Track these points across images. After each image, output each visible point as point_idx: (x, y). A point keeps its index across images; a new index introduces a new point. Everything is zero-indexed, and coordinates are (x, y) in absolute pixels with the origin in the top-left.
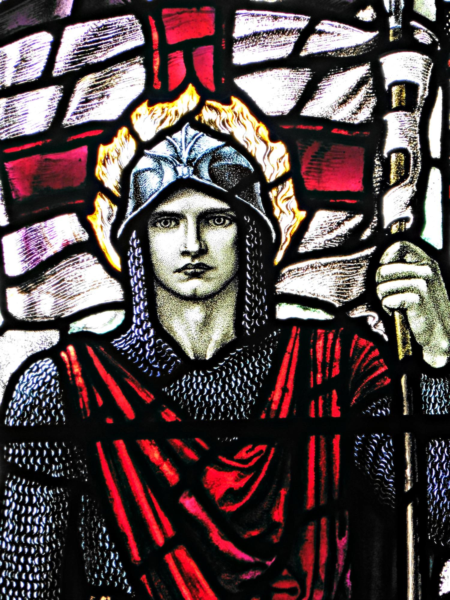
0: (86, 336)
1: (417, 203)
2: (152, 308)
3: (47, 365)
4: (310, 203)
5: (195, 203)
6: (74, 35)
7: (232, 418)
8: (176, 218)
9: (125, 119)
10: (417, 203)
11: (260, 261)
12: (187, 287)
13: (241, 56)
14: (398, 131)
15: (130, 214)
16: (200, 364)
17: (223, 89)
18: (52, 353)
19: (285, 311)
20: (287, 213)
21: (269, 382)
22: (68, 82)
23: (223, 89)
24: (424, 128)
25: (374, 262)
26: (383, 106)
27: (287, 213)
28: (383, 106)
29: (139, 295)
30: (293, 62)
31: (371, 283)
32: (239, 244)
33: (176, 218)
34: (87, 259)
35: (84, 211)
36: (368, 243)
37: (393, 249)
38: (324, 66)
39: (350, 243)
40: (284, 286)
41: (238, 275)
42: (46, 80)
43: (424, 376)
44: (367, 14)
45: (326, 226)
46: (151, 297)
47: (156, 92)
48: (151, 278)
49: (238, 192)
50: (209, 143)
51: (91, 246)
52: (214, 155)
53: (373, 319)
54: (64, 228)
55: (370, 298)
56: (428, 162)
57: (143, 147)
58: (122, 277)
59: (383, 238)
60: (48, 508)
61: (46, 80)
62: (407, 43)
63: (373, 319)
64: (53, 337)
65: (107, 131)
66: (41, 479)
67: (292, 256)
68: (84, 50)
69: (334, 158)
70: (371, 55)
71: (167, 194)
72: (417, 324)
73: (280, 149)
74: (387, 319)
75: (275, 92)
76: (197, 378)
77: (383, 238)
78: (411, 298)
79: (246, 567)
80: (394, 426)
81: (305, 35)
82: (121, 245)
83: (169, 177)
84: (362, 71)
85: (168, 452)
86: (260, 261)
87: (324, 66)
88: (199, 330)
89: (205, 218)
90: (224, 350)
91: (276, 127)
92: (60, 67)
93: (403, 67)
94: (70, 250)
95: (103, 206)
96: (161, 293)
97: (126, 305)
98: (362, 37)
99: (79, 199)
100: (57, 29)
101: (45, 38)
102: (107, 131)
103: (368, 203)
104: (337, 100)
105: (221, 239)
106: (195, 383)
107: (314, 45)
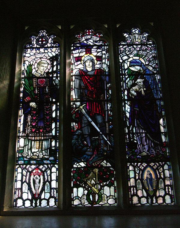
0: (81, 70)
1: (105, 61)
2: (86, 68)
3: (78, 71)
4: (97, 61)
5: (89, 61)
6: (80, 50)
7: (132, 140)
8: (87, 62)
9: (84, 56)
10: (105, 61)
11: (94, 65)
12: (88, 66)
13: (92, 52)
14: (104, 56)
15: (84, 61)
16: (89, 72)
17: (91, 53)
18: (79, 71)
19: (96, 68)
20: (96, 61)
21: (95, 73)
22: (80, 53)
23: (91, 53)
24: (106, 56)
25: (102, 65)
26: (103, 54)
27: (96, 61)
28: (103, 54)
29: (85, 67)
30: (96, 52)
31: (102, 66)
32: (92, 64)
33: (87, 62)
34: (81, 64)
35: (81, 61)
36: (101, 64)
37: (104, 64)
38: (98, 52)
39: (100, 63)
40: (95, 66)
41: (92, 66)
42: (78, 53)
43: (163, 188)
44: (101, 49)
45: (99, 62)
46: (86, 67)
47: (86, 54)
48: (86, 66)
49: (92, 60)
50: (90, 57)
51: (81, 64)
52: (90, 58)
53: (102, 68)
54: (79, 62)
55: (102, 67)
56: (106, 58)
57: (85, 57)
58: (84, 66)
59: (103, 63)
60: (97, 103)
61: (78, 53)
62: (104, 51)
63: (102, 68)
64: (78, 70)
65: (82, 56)
66: (78, 79)
67: (96, 64)
68: (81, 51)
69: (99, 58)
70: (102, 51)
71: (87, 60)
72: (105, 69)
73: (95, 57)
74: (103, 68)
75: (95, 54)
76: (89, 72)
77: (103, 63)
78: (105, 67)
79: (93, 85)
80: (104, 75)
81: (97, 50)
82: (84, 64)
83: (87, 59)
84: (101, 52)
85: (87, 77)
86: (94, 65)
87: (98, 52)
88: (89, 69)
89: (90, 62)
90: (91, 71)
91: (95, 56)
92: (79, 52)
93: (104, 52)
94: (80, 64)
95: (82, 61)
96: (86, 67)
97: (84, 67)
98: (101, 50)
99: (81, 60)
100: (79, 50)
101: (78, 50)
102: (82, 56)
103: (101, 61)
104: (99, 54)
105: (91, 63)
106: (89, 73)
107: (97, 51)
